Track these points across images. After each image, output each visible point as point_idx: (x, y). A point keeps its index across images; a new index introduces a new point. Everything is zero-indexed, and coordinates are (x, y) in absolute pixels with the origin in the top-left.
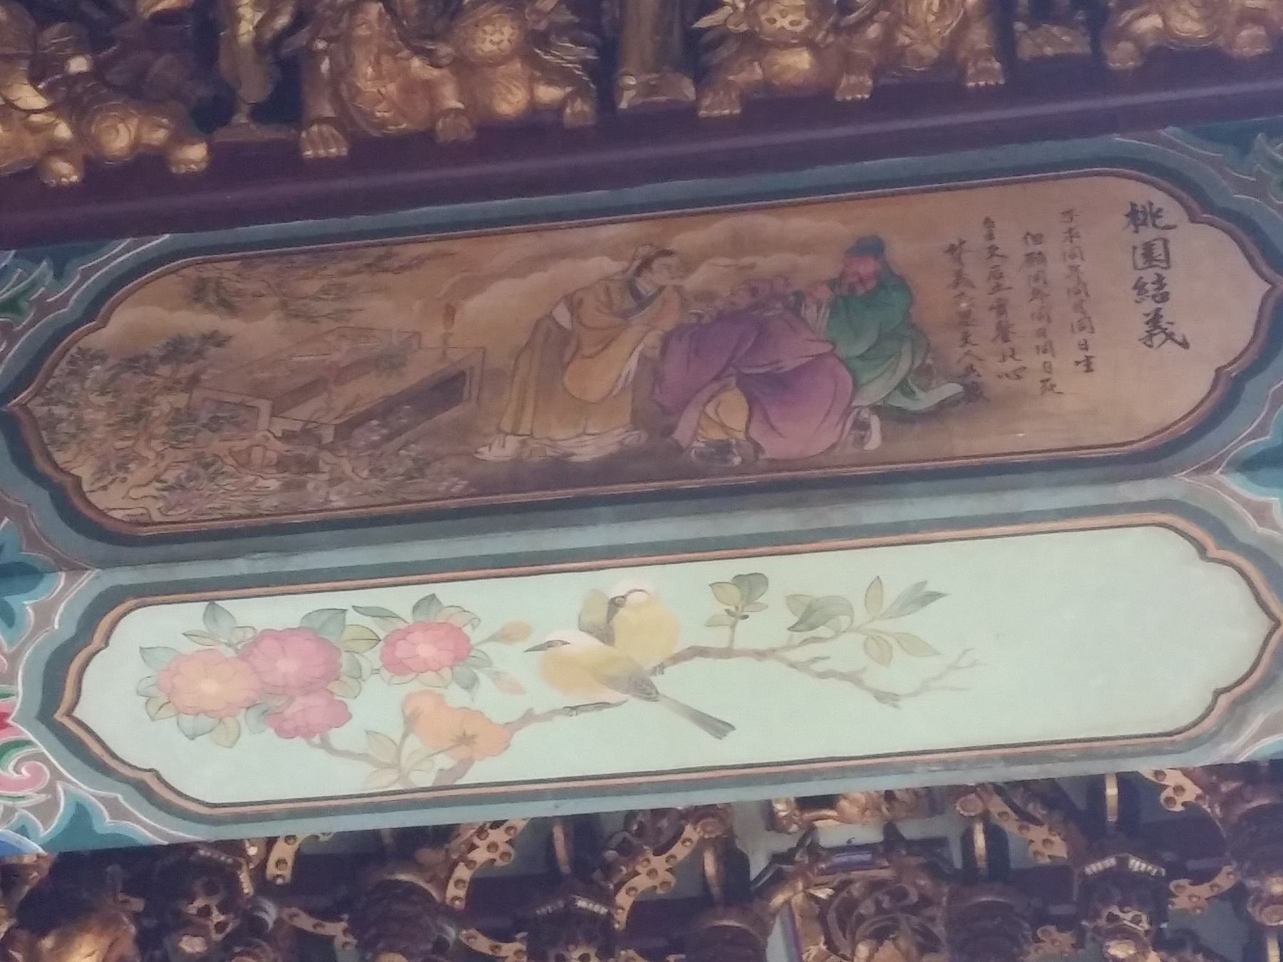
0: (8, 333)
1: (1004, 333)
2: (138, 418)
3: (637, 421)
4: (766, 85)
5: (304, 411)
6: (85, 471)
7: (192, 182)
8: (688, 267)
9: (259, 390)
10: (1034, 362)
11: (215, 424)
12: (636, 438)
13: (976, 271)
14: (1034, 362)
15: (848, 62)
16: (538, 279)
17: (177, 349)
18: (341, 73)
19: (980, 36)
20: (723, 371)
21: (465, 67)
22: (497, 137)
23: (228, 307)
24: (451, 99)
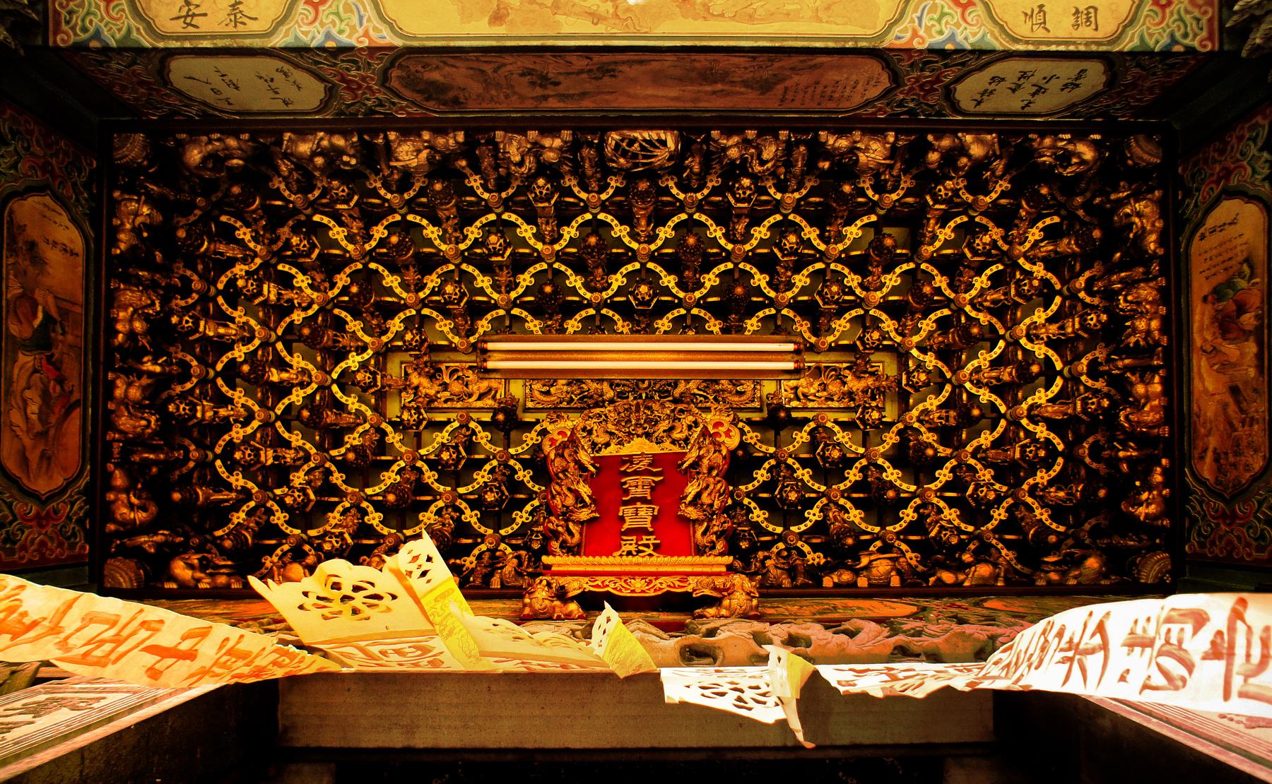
0: (32, 4)
1: (1230, 259)
2: (1234, 465)
3: (1247, 340)
4: (1159, 330)
5: (1235, 422)
6: (1248, 475)
7: (1172, 462)
8: (1205, 340)
9: (1229, 436)
10: (1239, 248)
11: (1238, 445)
12: (1252, 339)
13: (1213, 270)
14: (1239, 248)
15: (1156, 312)
16: (1205, 376)
17: (1216, 459)
18: (1146, 425)
19: (1151, 284)
20: (1251, 484)
21: (1148, 398)
22: (1167, 391)
23: (1205, 450)
24: (1156, 402)
